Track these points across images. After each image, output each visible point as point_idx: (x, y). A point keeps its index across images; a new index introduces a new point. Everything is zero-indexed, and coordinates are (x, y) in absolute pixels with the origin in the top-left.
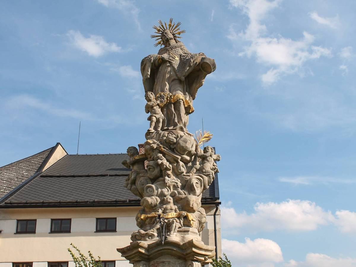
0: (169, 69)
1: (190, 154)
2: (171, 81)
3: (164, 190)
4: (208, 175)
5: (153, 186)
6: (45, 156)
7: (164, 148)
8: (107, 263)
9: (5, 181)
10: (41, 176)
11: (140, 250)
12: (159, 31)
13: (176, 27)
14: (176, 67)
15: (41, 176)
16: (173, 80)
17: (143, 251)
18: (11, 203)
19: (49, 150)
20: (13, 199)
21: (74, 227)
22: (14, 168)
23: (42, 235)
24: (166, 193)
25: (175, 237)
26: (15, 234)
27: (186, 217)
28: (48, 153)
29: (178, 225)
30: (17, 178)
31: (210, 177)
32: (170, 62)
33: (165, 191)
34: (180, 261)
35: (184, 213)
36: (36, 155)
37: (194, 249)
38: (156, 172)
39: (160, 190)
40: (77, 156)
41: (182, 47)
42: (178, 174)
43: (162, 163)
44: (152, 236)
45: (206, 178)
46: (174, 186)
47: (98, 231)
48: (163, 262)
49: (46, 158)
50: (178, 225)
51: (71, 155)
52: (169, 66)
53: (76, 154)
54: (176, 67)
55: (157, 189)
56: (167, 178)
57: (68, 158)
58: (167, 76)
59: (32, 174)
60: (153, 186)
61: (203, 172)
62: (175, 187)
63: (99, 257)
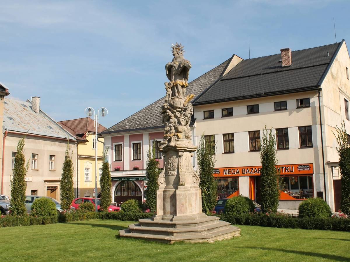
0: (174, 69)
1: (179, 108)
2: (176, 75)
3: (171, 124)
4: (187, 117)
5: (167, 123)
6: (225, 65)
7: (169, 107)
8: (306, 127)
9: (201, 86)
10: (221, 80)
11: (160, 149)
12: (177, 45)
13: (180, 45)
14: (177, 68)
15: (221, 80)
16: (176, 74)
17: (162, 149)
18: (198, 102)
19: (228, 61)
20: (200, 100)
21: (235, 112)
22: (207, 76)
23: (218, 119)
24: (172, 126)
25: (172, 144)
26: (203, 119)
27: (177, 135)
28: (227, 62)
29: (174, 138)
30: (208, 83)
31: (188, 117)
32: (174, 66)
33: (171, 125)
34: (176, 152)
35: (176, 134)
36: (203, 76)
37: (177, 148)
38: (167, 117)
39: (169, 124)
40: (250, 59)
41: (180, 57)
42: (176, 117)
43: (168, 114)
44: (165, 143)
45: (187, 118)
46: (175, 122)
47: (276, 110)
48: (170, 153)
49: (226, 66)
50: (174, 138)
51: (245, 60)
52: (174, 68)
53: (249, 59)
54: (177, 68)
55: (168, 124)
56: (171, 119)
57: (244, 63)
58: (174, 72)
59: (217, 78)
60: (167, 123)
61: (185, 116)
62: (175, 123)
63: (272, 127)
